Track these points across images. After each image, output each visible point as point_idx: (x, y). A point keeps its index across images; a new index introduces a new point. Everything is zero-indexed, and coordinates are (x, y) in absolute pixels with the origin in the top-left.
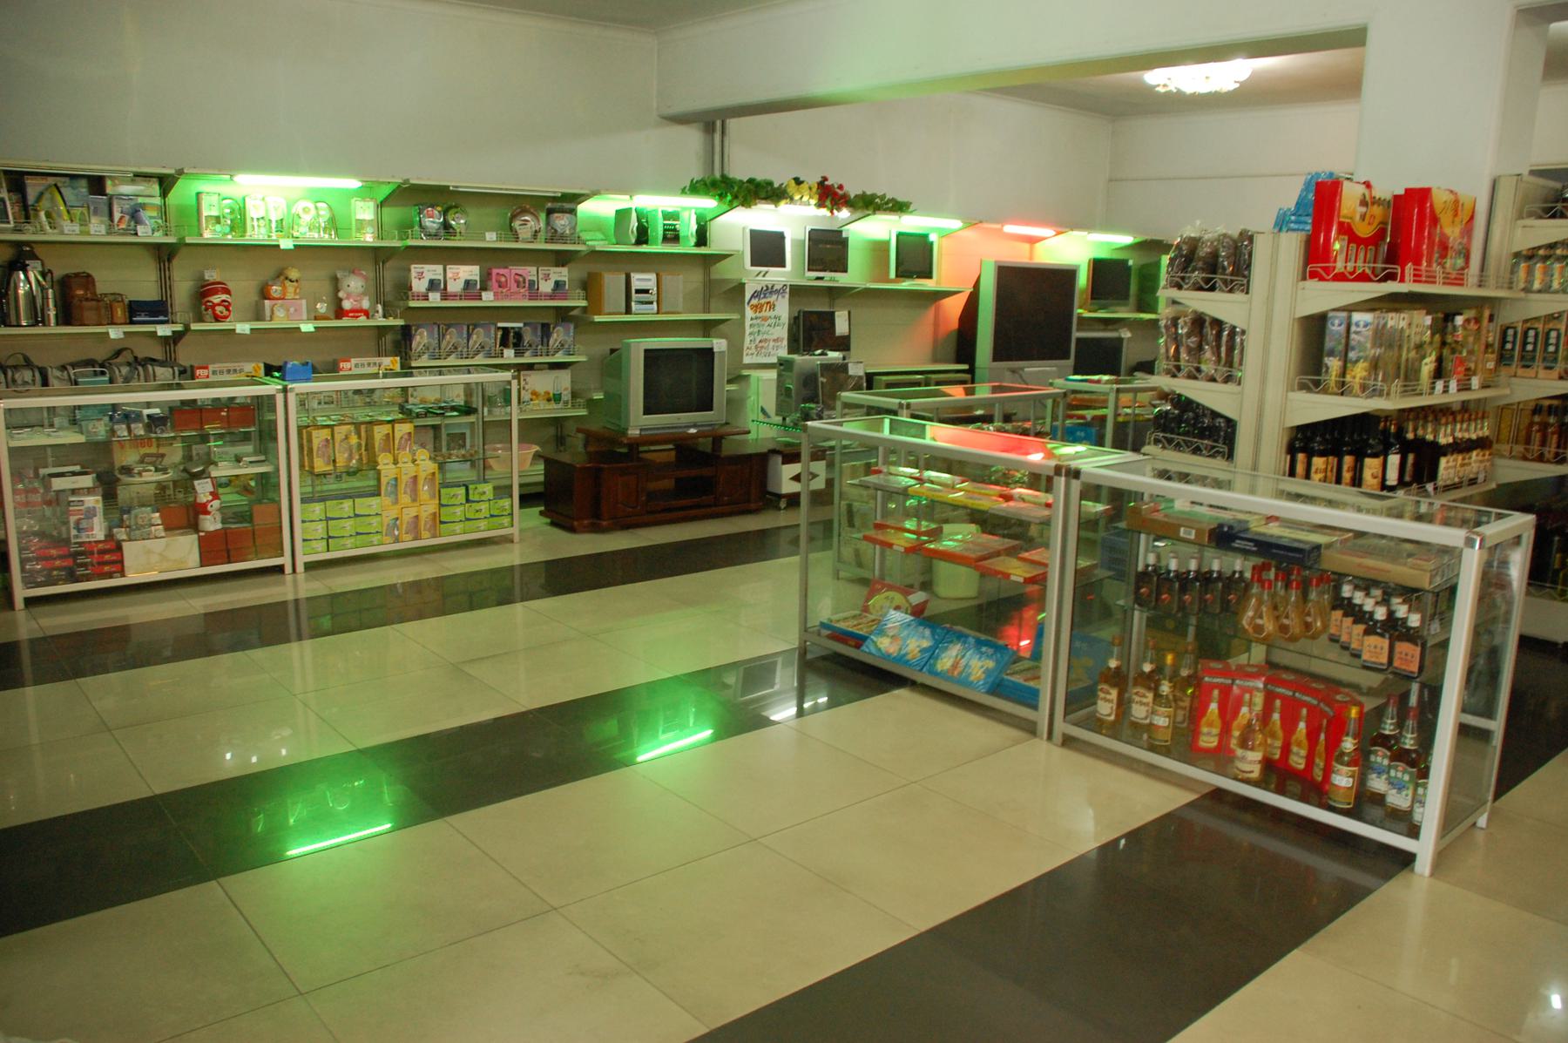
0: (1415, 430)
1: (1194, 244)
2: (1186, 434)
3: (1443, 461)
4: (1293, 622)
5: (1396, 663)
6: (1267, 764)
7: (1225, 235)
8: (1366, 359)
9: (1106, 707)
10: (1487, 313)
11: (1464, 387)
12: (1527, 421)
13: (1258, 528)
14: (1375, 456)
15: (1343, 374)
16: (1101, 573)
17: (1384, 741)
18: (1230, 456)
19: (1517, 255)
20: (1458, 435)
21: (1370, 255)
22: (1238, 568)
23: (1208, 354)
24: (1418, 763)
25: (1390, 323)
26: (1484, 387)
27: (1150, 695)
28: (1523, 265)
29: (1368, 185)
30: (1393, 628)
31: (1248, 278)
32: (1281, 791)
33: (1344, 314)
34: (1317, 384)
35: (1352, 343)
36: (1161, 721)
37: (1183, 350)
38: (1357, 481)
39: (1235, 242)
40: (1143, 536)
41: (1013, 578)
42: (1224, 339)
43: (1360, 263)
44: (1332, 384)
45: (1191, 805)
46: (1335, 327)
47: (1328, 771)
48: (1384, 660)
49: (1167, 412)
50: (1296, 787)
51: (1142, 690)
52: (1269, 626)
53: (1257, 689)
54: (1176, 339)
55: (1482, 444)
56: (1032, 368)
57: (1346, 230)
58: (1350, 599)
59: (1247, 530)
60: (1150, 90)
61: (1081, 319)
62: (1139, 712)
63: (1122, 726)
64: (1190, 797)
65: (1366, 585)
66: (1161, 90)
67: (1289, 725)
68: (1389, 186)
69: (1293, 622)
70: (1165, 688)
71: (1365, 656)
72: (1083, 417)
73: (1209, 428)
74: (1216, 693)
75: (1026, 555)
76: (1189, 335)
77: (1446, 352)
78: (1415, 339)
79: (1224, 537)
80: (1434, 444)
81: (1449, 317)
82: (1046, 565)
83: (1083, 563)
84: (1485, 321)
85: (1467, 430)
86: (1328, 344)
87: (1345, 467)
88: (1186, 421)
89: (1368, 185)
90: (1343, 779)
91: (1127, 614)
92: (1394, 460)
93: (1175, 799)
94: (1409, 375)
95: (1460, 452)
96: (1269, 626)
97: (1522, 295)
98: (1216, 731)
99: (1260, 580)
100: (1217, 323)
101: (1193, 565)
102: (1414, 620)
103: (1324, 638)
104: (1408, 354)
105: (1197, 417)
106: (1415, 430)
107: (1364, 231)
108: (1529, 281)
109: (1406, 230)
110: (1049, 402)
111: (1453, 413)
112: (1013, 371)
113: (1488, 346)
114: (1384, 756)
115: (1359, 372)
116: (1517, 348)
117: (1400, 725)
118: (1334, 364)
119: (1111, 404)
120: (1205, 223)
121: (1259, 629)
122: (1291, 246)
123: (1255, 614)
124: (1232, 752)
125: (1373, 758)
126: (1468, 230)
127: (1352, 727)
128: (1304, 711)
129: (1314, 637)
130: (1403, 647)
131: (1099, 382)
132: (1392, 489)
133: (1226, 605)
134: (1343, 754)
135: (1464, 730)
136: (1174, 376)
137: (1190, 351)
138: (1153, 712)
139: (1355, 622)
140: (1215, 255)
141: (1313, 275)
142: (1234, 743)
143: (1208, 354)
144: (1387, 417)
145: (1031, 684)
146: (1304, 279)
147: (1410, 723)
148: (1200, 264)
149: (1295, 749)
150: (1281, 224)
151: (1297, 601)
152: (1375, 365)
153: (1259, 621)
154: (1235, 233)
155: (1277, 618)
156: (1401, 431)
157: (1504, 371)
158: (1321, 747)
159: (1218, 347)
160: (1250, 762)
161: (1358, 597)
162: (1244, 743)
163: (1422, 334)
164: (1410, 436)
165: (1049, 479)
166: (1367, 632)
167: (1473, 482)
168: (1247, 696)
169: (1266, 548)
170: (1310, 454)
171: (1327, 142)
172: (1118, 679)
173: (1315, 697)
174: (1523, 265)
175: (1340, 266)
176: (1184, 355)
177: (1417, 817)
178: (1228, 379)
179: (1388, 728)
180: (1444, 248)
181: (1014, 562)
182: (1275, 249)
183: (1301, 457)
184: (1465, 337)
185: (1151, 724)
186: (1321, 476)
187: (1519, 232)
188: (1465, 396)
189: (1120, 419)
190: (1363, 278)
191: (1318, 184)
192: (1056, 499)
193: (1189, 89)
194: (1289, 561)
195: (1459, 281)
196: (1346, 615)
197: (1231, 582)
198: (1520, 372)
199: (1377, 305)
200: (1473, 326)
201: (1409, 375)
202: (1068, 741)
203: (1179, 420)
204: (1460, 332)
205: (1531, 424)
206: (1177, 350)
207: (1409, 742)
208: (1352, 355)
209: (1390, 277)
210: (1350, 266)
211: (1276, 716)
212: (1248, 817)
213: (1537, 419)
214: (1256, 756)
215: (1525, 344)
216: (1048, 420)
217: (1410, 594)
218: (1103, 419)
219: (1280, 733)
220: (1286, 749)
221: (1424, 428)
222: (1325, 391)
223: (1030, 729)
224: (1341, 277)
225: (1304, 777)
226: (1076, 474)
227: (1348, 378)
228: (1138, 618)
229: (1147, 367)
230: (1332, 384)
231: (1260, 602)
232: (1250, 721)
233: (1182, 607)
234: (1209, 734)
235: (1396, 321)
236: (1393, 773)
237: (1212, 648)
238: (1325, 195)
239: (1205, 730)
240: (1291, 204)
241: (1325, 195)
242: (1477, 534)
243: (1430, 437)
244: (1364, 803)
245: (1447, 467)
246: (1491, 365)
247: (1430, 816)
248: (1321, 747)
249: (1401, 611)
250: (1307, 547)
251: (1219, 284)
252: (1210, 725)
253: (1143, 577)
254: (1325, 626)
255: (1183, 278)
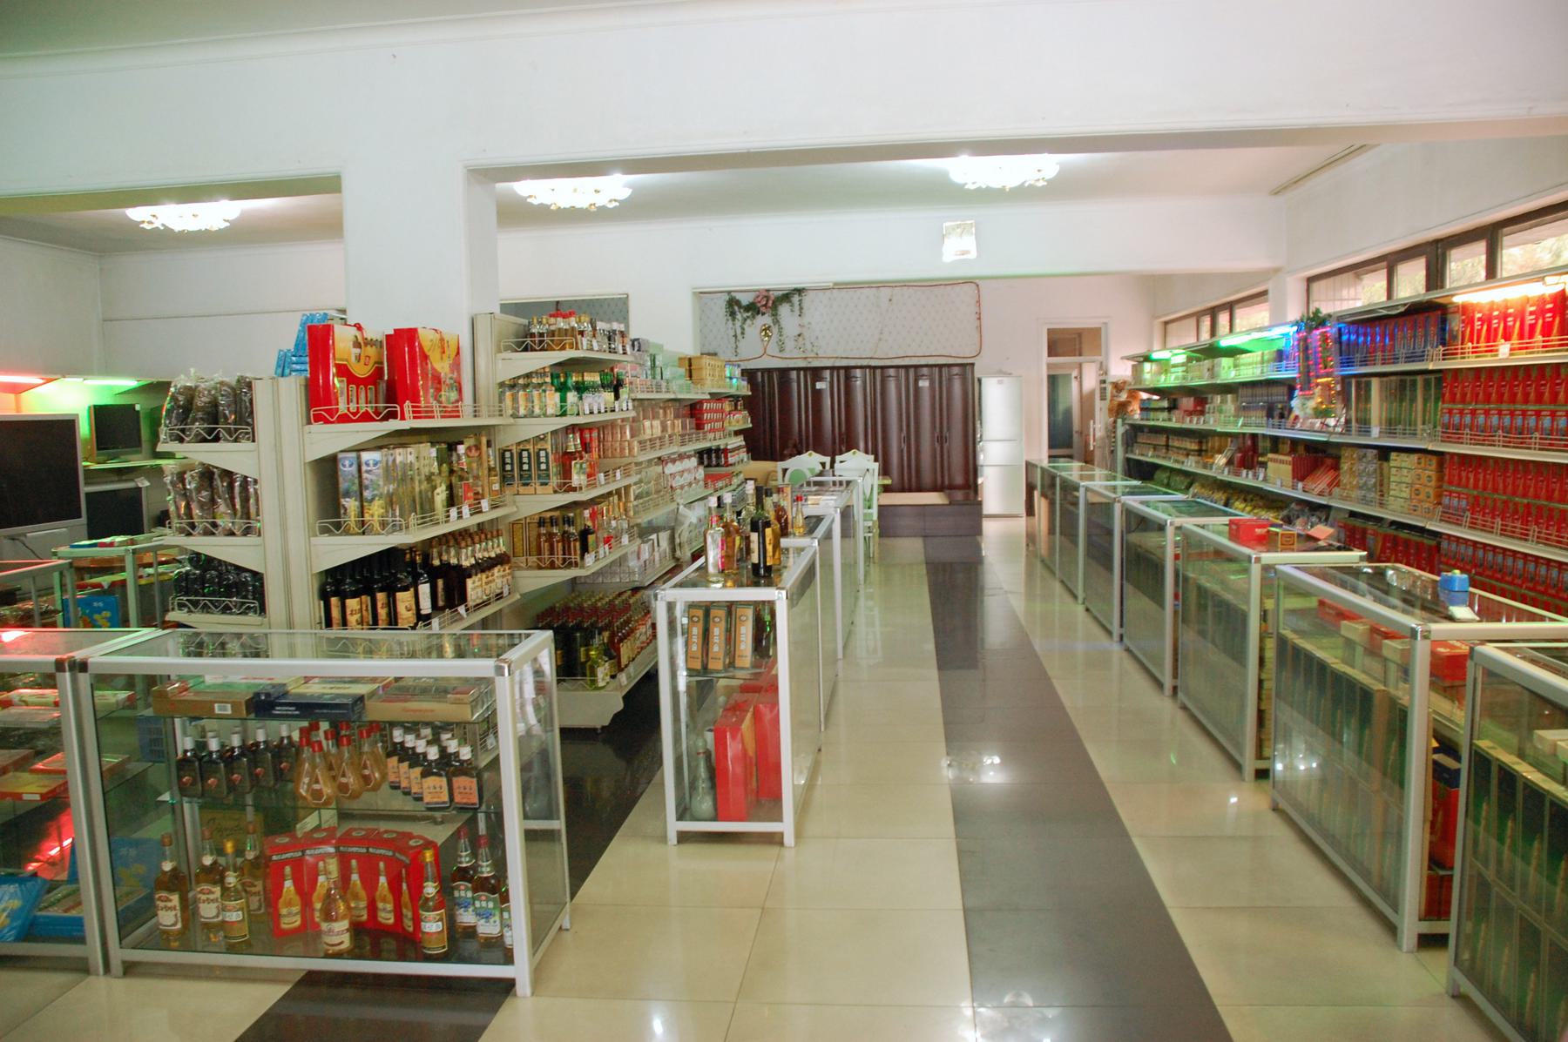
0: (440, 555)
1: (190, 393)
2: (210, 594)
3: (469, 582)
4: (351, 780)
5: (457, 798)
6: (357, 929)
7: (222, 383)
8: (381, 497)
9: (168, 916)
10: (484, 440)
11: (477, 511)
12: (534, 533)
13: (298, 690)
14: (406, 589)
15: (362, 514)
16: (136, 767)
17: (463, 874)
18: (262, 610)
19: (502, 385)
20: (479, 555)
21: (371, 395)
22: (284, 734)
23: (222, 507)
24: (496, 887)
25: (399, 459)
26: (494, 507)
27: (217, 890)
28: (508, 393)
29: (359, 327)
30: (447, 765)
31: (252, 426)
32: (377, 955)
33: (354, 455)
34: (338, 526)
35: (366, 482)
36: (234, 916)
37: (194, 506)
38: (393, 620)
39: (233, 389)
40: (177, 721)
41: (26, 797)
42: (237, 490)
43: (362, 404)
44: (353, 525)
45: (287, 995)
46: (347, 468)
47: (417, 921)
48: (446, 798)
49: (187, 573)
50: (389, 944)
51: (205, 887)
52: (328, 790)
53: (329, 855)
54: (185, 495)
55: (501, 560)
56: (36, 533)
57: (343, 371)
58: (402, 743)
59: (286, 694)
60: (136, 225)
61: (87, 471)
62: (208, 911)
63: (192, 932)
64: (285, 989)
65: (412, 728)
66: (147, 227)
67: (370, 884)
68: (378, 329)
69: (351, 780)
70: (231, 879)
71: (427, 799)
72: (99, 585)
73: (236, 584)
74: (288, 870)
75: (40, 766)
76: (198, 490)
77: (454, 480)
78: (425, 471)
79: (263, 705)
80: (459, 566)
81: (452, 447)
82: (64, 772)
83: (111, 760)
84: (484, 447)
85: (486, 550)
86: (343, 485)
87: (379, 605)
88: (211, 581)
89: (359, 327)
90: (433, 925)
91: (175, 810)
92: (425, 589)
93: (267, 996)
94: (424, 507)
95: (483, 571)
96: (328, 790)
97: (512, 420)
98: (296, 909)
99: (309, 743)
100: (228, 475)
101: (236, 741)
102: (466, 753)
103: (385, 787)
104: (419, 487)
105: (220, 575)
106: (440, 555)
107: (361, 371)
108: (516, 409)
109: (399, 370)
110: (56, 575)
111: (471, 535)
112: (13, 538)
113: (490, 469)
114: (467, 889)
115: (376, 510)
116: (515, 469)
117: (474, 855)
118: (351, 504)
119: (129, 563)
120: (201, 370)
121: (317, 794)
122: (292, 390)
123: (311, 781)
124: (317, 926)
125: (456, 894)
126: (456, 365)
127: (430, 870)
128: (382, 865)
129: (376, 789)
130: (461, 782)
131: (111, 545)
132: (428, 617)
133: (280, 775)
134: (427, 899)
135: (531, 836)
136: (189, 534)
137: (202, 506)
138: (224, 909)
139: (411, 766)
140: (215, 404)
141: (318, 418)
142: (317, 916)
143: (222, 507)
144: (412, 548)
145: (74, 913)
146: (309, 423)
147: (483, 851)
148: (200, 415)
149: (380, 905)
150: (283, 367)
151: (351, 757)
152: (390, 501)
153: (316, 787)
154: (232, 381)
155: (334, 778)
156: (427, 557)
157: (508, 491)
158: (406, 897)
159: (232, 498)
160: (338, 933)
161: (410, 741)
162: (328, 917)
163: (431, 465)
164: (436, 562)
165: (52, 677)
166: (425, 774)
167: (499, 596)
168: (321, 864)
169: (309, 709)
170: (343, 597)
171: (315, 282)
172: (177, 882)
173: (388, 848)
174: (508, 393)
175: (342, 407)
176: (196, 512)
177: (508, 941)
178: (247, 531)
179: (465, 861)
180: (437, 379)
181: (26, 776)
182: (276, 394)
183: (334, 600)
184: (469, 464)
185: (224, 922)
186: (357, 616)
187: (500, 364)
188: (479, 519)
189: (143, 582)
190: (366, 418)
191: (310, 328)
192: (63, 694)
193: (177, 227)
194: (341, 718)
195: (455, 414)
196: (401, 761)
197: (282, 751)
198: (522, 489)
199: (396, 440)
200: (474, 453)
201: (424, 507)
202: (130, 969)
203: (202, 580)
204: (464, 459)
205: (539, 536)
206: (188, 507)
207: (486, 870)
208: (367, 494)
209: (392, 415)
210: (353, 407)
211: (355, 877)
212: (350, 992)
213: (543, 531)
214: (344, 925)
215: (521, 464)
216: (57, 594)
217: (460, 728)
218: (123, 583)
219: (363, 894)
220: (372, 908)
221: (448, 552)
222: (347, 533)
223: (82, 968)
224: (344, 419)
225: (396, 931)
226: (83, 666)
227: (367, 517)
228: (189, 809)
229: (162, 519)
230: (353, 525)
231: (314, 767)
232: (329, 890)
233: (232, 787)
234: (289, 914)
235: (402, 456)
236: (477, 904)
237: (279, 821)
238: (318, 339)
239: (284, 911)
240: (289, 345)
241: (318, 339)
242: (504, 661)
243: (454, 561)
244: (460, 942)
245: (475, 588)
246: (496, 487)
247: (519, 937)
248: (406, 897)
249: (453, 746)
250: (349, 701)
251: (223, 434)
252: (289, 904)
253: (184, 763)
254: (384, 776)
255: (183, 431)
